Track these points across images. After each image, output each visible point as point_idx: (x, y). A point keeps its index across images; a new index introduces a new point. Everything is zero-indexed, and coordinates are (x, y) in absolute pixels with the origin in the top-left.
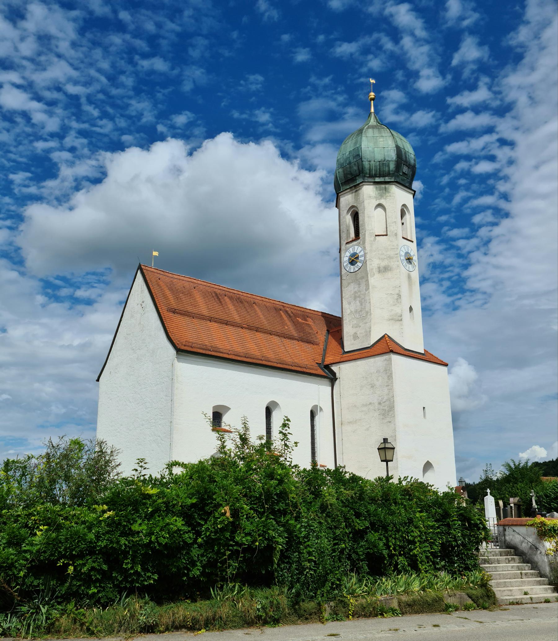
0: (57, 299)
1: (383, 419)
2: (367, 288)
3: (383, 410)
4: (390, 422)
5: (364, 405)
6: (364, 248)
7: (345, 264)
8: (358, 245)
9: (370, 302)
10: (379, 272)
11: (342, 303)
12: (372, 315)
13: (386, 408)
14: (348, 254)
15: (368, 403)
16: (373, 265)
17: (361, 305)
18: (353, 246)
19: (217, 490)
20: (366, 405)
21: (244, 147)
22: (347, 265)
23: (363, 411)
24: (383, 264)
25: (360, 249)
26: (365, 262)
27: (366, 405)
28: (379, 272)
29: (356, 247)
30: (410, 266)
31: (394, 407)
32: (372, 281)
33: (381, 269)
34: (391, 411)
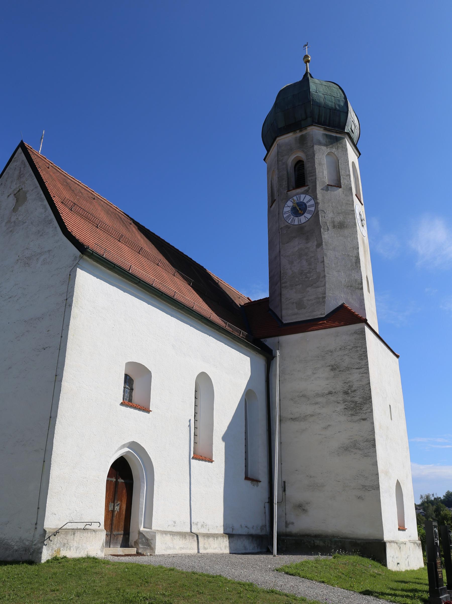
0: (293, 596)
1: (352, 415)
2: (320, 245)
4: (364, 419)
5: (318, 395)
6: (315, 198)
7: (285, 216)
8: (306, 193)
12: (327, 278)
13: (357, 399)
15: (326, 392)
16: (326, 218)
17: (310, 264)
18: (297, 194)
19: (93, 565)
20: (323, 395)
22: (288, 217)
25: (308, 198)
26: (316, 215)
27: (323, 395)
29: (303, 196)
30: (315, 247)
32: (326, 236)
33: (336, 224)
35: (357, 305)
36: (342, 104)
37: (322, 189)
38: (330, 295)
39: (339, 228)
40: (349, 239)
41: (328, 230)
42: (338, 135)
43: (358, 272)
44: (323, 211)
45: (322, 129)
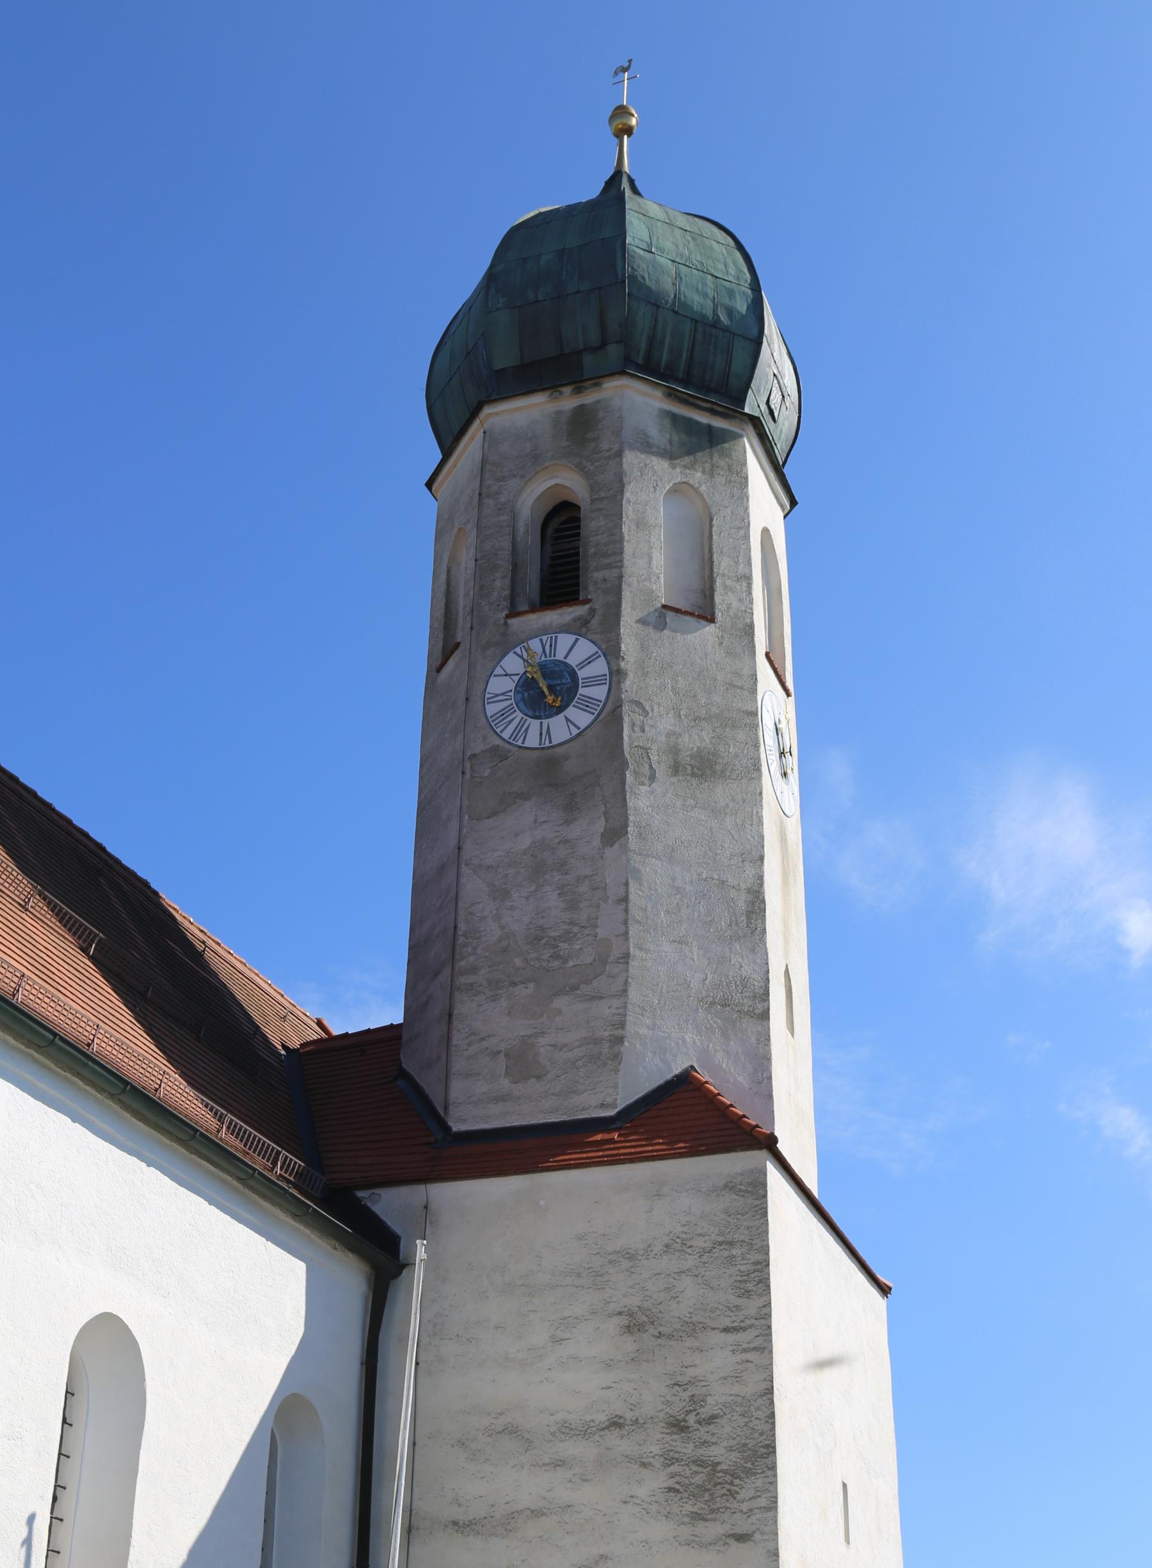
1: (696, 1517)
2: (615, 833)
3: (700, 1463)
4: (742, 1538)
6: (612, 652)
8: (580, 628)
9: (625, 899)
10: (676, 769)
11: (799, 418)
12: (634, 964)
14: (513, 664)
15: (602, 1418)
16: (650, 732)
17: (573, 906)
20: (585, 1432)
21: (398, 1231)
23: (559, 1463)
24: (696, 740)
25: (585, 648)
27: (585, 1432)
28: (676, 769)
31: (771, 1449)
32: (642, 801)
33: (685, 758)
34: (749, 1472)
35: (743, 1079)
36: (742, 306)
37: (642, 621)
38: (643, 1031)
39: (693, 775)
40: (729, 821)
41: (652, 778)
42: (718, 423)
43: (753, 951)
44: (639, 704)
45: (658, 393)
